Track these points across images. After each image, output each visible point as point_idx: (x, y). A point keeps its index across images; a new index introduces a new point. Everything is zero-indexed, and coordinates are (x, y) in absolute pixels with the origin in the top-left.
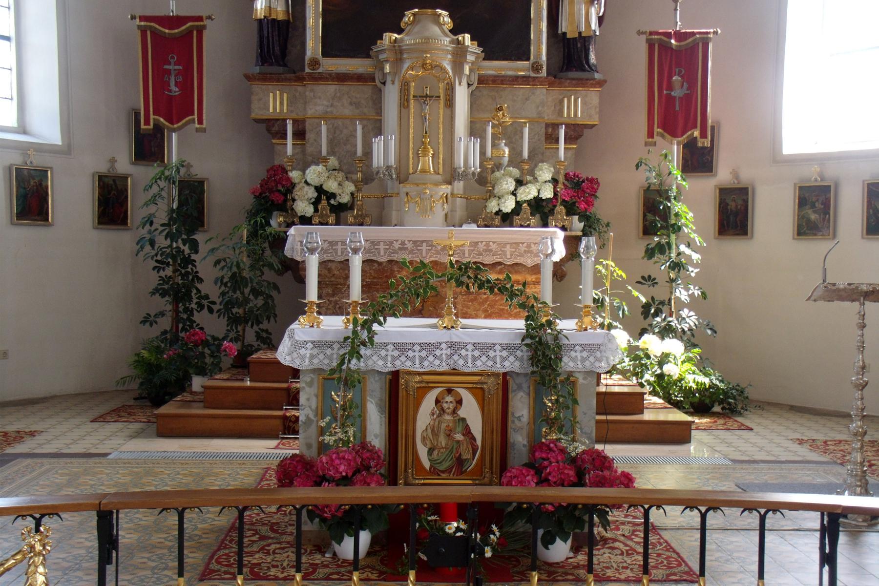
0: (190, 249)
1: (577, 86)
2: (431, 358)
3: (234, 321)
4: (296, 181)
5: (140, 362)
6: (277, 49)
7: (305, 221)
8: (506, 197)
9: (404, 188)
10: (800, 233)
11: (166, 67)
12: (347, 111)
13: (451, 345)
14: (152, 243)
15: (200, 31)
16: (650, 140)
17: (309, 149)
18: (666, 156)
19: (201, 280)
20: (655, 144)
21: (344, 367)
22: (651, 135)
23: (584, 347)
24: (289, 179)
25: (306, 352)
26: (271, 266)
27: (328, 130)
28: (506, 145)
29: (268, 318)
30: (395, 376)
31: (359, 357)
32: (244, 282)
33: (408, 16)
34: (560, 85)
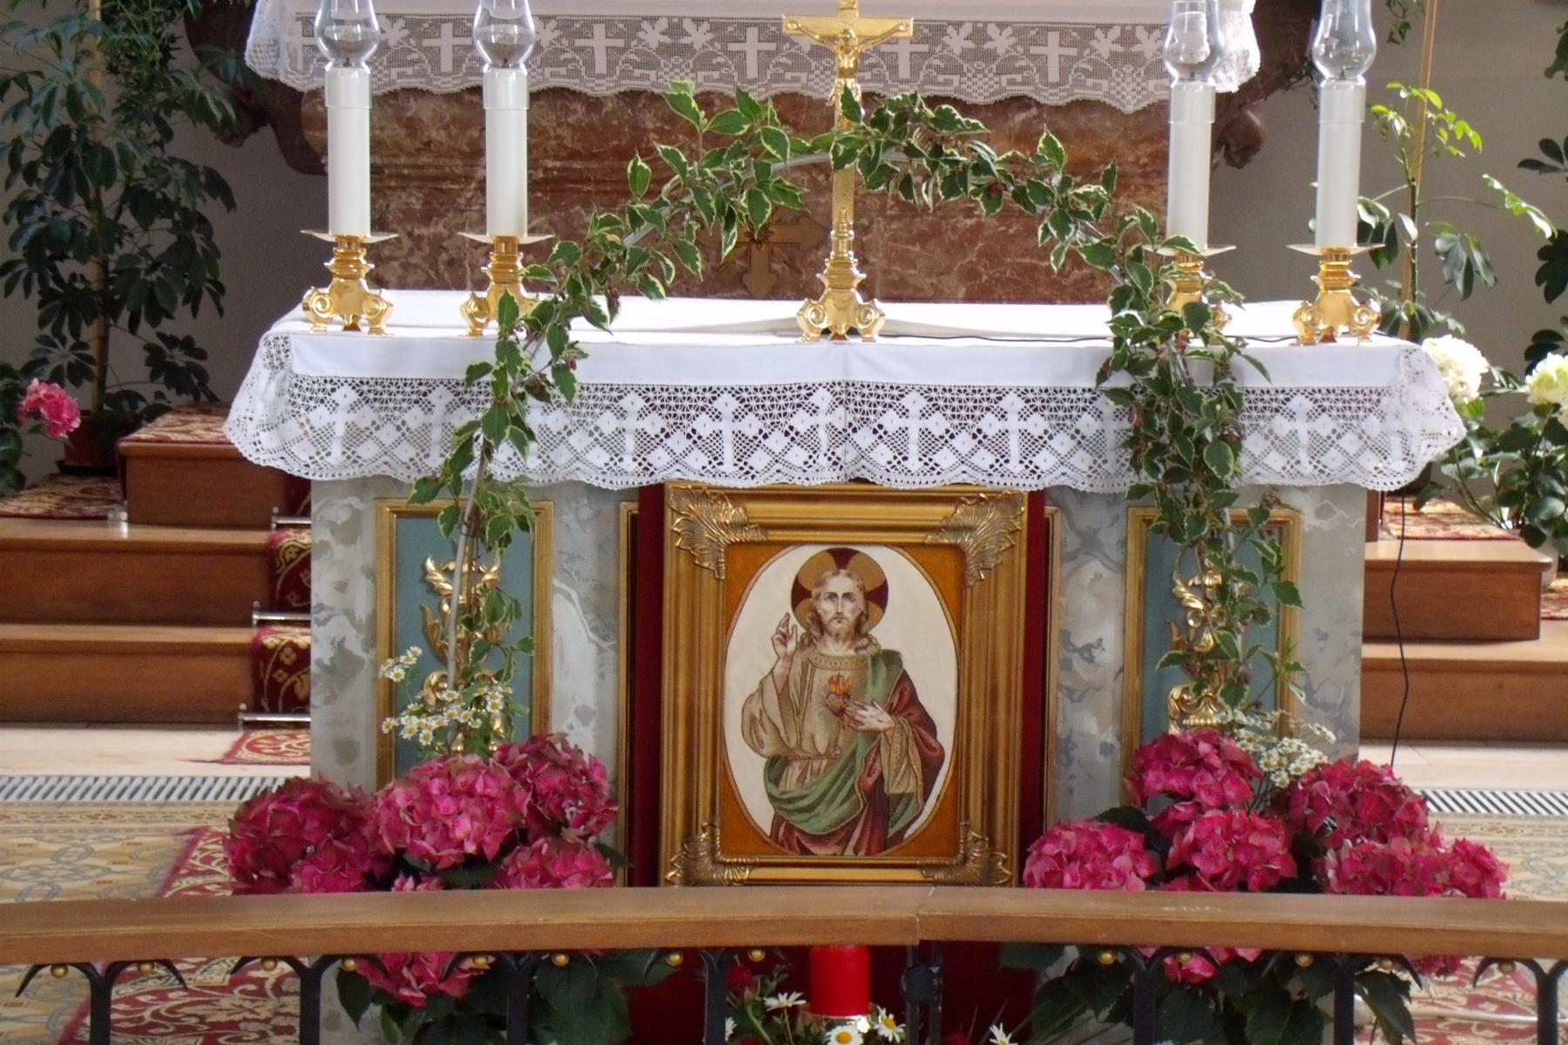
13: (845, 393)
21: (470, 472)
23: (1321, 401)
25: (335, 418)
26: (197, 108)
29: (193, 299)
30: (652, 500)
31: (524, 436)
32: (103, 165)
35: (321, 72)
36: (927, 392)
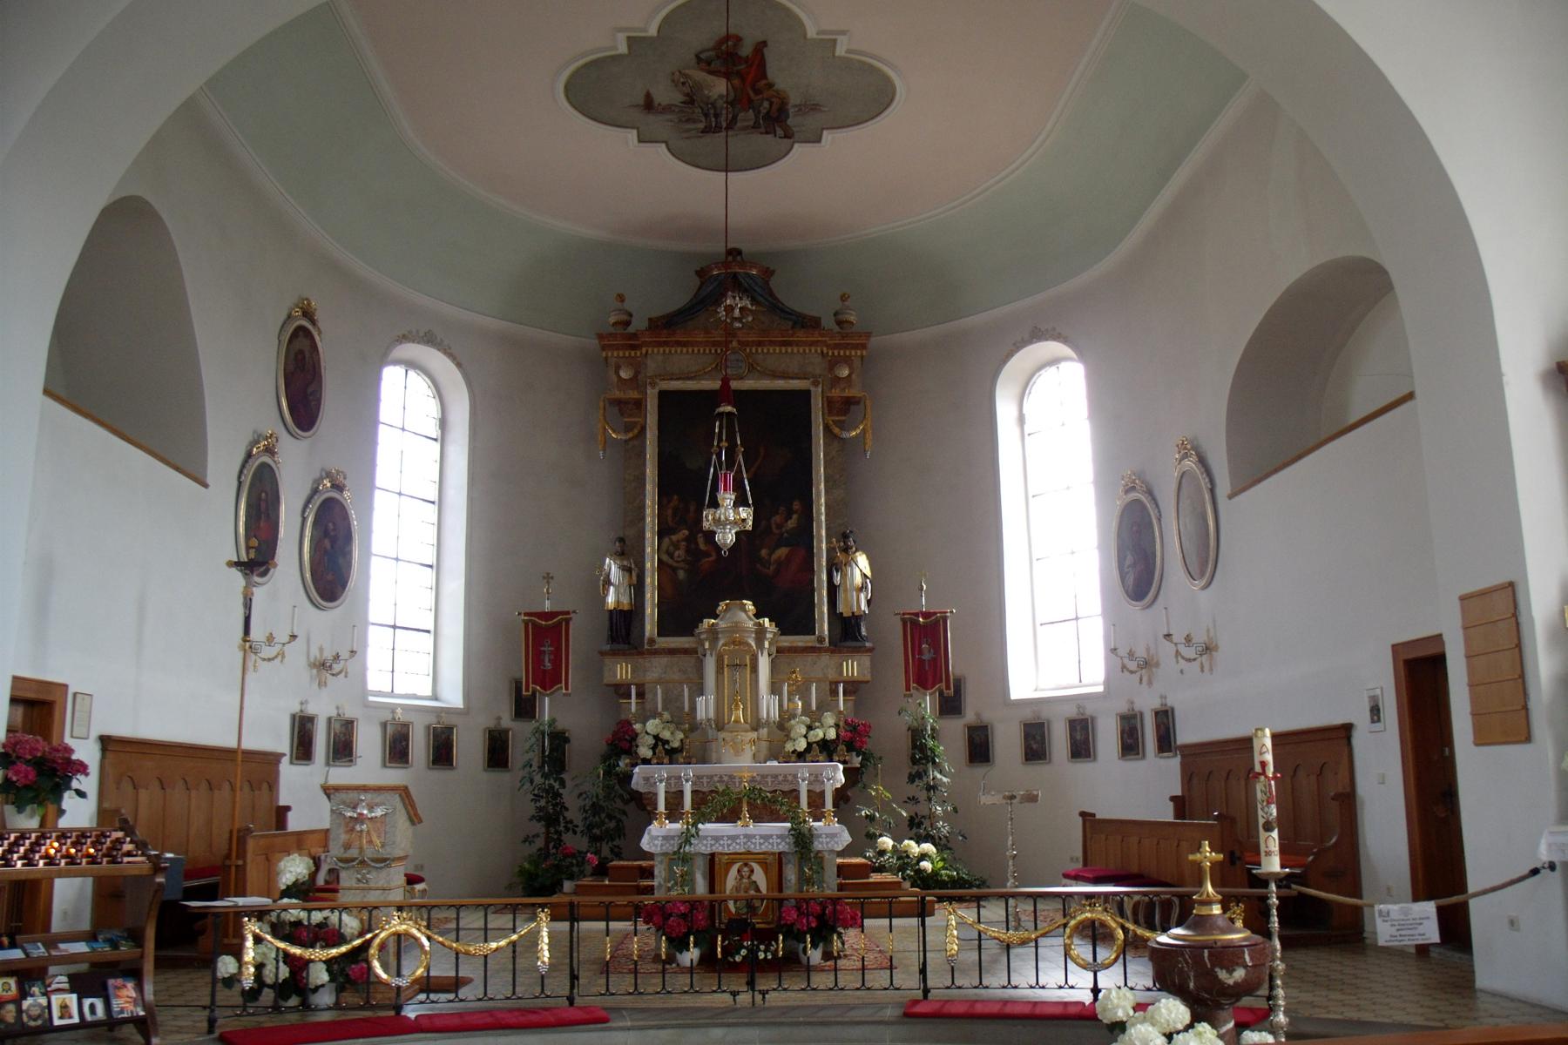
0: (560, 785)
1: (852, 652)
2: (734, 844)
3: (594, 839)
4: (639, 731)
5: (522, 872)
6: (623, 631)
7: (646, 761)
8: (800, 739)
9: (722, 735)
10: (1027, 760)
11: (542, 649)
12: (676, 676)
13: (746, 836)
14: (532, 781)
15: (567, 621)
16: (908, 693)
17: (648, 706)
18: (920, 704)
19: (567, 809)
20: (911, 696)
21: (682, 851)
22: (908, 689)
23: (827, 835)
24: (633, 730)
25: (658, 843)
26: (621, 796)
27: (662, 693)
28: (799, 699)
29: (620, 837)
30: (713, 855)
31: (691, 844)
32: (602, 809)
33: (722, 606)
34: (840, 652)
35: (682, 785)
36: (760, 835)
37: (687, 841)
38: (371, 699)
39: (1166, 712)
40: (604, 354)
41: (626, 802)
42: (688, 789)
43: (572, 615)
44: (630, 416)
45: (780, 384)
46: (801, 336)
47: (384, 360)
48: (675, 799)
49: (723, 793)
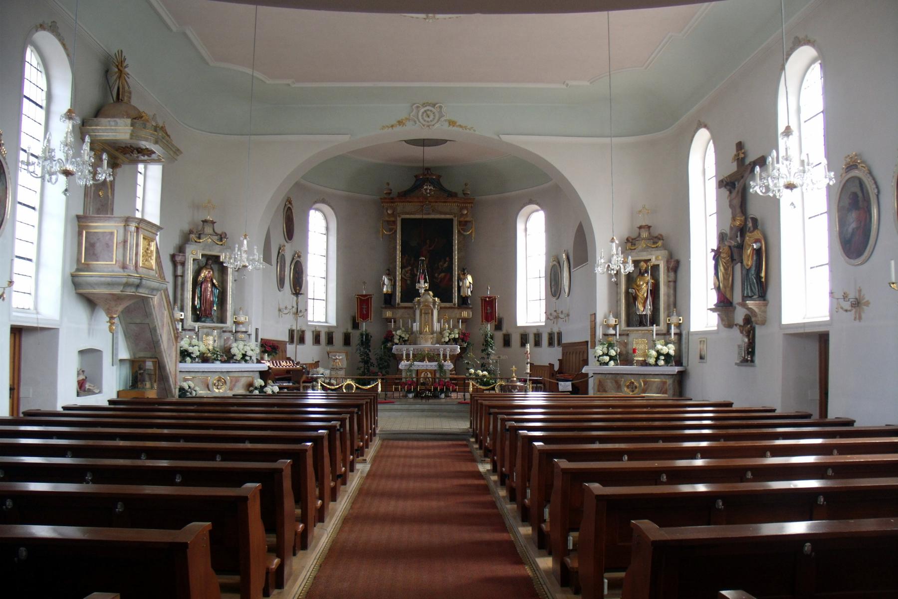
3: (380, 368)
7: (397, 344)
9: (421, 336)
14: (360, 350)
15: (371, 298)
17: (397, 325)
22: (482, 322)
24: (393, 334)
25: (404, 366)
37: (411, 366)
38: (309, 323)
39: (559, 333)
40: (382, 205)
41: (389, 357)
42: (411, 353)
43: (372, 296)
44: (392, 226)
45: (443, 217)
46: (450, 199)
47: (311, 208)
48: (408, 355)
49: (421, 354)
